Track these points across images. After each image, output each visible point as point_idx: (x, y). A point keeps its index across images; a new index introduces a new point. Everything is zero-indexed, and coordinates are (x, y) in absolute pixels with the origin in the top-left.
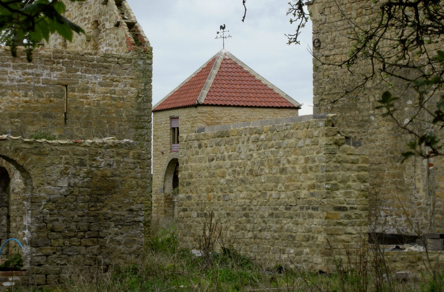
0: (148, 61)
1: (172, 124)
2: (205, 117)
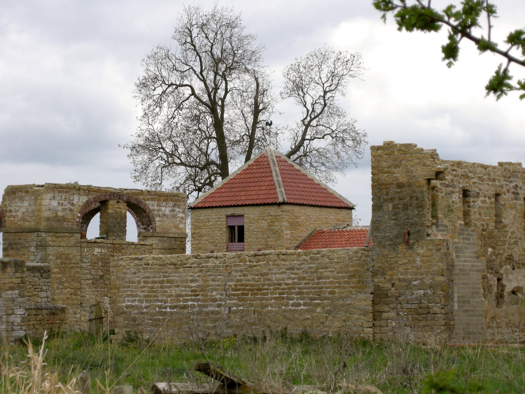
0: (375, 184)
1: (229, 222)
2: (288, 215)
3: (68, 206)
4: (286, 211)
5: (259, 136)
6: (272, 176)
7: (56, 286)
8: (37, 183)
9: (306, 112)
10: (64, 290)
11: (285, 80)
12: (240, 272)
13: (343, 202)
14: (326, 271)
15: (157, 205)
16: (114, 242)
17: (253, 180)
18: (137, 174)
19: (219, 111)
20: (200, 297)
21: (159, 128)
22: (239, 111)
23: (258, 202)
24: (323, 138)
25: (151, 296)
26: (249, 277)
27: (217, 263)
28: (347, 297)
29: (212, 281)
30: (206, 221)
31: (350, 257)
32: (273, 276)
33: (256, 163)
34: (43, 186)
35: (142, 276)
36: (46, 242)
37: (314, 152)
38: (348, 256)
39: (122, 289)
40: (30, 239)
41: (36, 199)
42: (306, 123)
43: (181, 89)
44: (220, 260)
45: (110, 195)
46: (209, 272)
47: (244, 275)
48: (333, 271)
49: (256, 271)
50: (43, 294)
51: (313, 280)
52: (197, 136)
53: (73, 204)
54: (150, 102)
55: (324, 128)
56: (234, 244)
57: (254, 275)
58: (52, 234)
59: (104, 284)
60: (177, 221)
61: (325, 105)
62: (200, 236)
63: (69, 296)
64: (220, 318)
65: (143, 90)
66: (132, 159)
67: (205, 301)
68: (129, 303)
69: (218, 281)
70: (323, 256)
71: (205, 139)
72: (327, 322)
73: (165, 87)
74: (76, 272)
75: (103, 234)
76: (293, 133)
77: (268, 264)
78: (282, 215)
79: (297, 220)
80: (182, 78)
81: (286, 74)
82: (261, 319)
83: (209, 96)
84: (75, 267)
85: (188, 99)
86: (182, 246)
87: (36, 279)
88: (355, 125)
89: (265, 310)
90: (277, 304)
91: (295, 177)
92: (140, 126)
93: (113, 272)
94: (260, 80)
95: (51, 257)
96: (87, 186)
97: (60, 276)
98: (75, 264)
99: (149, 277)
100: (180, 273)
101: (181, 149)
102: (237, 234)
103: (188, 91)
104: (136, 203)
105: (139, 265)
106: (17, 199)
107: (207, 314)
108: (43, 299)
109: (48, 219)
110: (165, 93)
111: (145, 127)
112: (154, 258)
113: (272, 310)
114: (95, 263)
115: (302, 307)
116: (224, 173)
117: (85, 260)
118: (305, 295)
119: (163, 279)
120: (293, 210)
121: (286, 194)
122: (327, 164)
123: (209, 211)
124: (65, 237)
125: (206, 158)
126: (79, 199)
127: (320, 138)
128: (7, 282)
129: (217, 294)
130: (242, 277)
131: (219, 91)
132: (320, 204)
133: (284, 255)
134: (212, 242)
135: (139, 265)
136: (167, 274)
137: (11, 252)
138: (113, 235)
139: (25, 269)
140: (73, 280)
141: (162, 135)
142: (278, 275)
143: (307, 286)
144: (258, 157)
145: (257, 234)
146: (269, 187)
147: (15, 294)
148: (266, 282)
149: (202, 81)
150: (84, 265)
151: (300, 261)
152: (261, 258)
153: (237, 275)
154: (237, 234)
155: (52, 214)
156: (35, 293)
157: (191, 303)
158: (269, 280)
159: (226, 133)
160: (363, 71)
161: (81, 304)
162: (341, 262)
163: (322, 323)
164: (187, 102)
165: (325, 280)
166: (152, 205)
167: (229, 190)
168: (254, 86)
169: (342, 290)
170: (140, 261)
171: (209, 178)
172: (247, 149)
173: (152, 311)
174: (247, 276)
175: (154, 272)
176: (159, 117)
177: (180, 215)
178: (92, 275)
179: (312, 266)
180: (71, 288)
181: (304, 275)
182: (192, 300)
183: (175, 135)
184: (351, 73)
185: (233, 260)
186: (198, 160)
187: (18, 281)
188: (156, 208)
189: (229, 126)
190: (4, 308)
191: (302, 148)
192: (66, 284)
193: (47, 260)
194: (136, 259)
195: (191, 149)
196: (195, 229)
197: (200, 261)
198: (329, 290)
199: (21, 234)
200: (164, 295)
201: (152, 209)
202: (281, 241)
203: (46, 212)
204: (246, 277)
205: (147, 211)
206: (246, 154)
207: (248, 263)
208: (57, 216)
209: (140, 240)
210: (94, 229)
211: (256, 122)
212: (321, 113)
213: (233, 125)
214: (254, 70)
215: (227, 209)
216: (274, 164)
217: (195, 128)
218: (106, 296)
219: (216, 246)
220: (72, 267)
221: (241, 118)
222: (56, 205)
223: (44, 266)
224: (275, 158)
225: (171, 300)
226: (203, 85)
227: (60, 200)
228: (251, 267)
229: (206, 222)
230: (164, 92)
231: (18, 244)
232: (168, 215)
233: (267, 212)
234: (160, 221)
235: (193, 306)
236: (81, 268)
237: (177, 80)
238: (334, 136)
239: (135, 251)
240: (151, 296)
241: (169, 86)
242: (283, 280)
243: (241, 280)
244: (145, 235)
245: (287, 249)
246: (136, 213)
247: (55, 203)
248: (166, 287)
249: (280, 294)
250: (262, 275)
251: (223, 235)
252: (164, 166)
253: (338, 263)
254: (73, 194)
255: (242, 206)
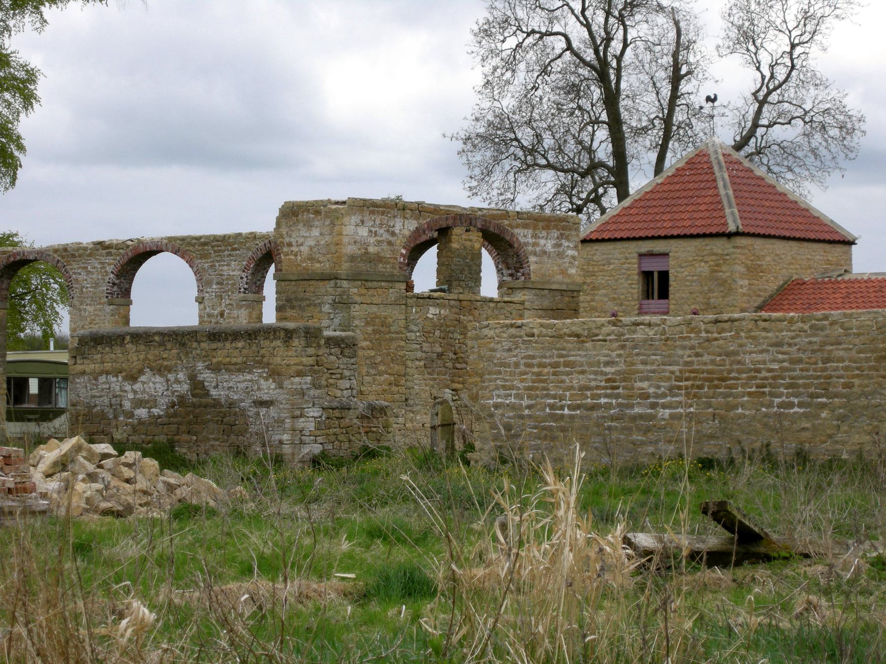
1: (643, 265)
2: (744, 254)
3: (386, 236)
4: (741, 247)
5: (680, 119)
6: (716, 188)
7: (364, 370)
8: (334, 198)
9: (760, 79)
10: (378, 377)
11: (725, 24)
12: (690, 349)
13: (837, 232)
14: (838, 349)
15: (532, 236)
16: (461, 297)
17: (684, 194)
18: (474, 184)
19: (612, 77)
20: (620, 391)
21: (510, 106)
22: (647, 77)
23: (694, 231)
24: (789, 123)
25: (537, 388)
26: (706, 358)
27: (651, 333)
28: (874, 393)
29: (642, 363)
30: (604, 262)
31: (879, 325)
32: (747, 356)
33: (690, 166)
34: (344, 203)
35: (523, 355)
36: (348, 295)
37: (776, 147)
38: (876, 323)
39: (487, 376)
40: (323, 291)
41: (333, 224)
42: (761, 98)
43: (549, 39)
44: (656, 328)
45: (455, 218)
46: (636, 348)
47: (697, 355)
48: (850, 349)
49: (718, 347)
50: (345, 384)
51: (816, 363)
52: (576, 119)
53: (393, 234)
54: (496, 61)
55: (792, 108)
56: (651, 301)
57: (714, 354)
58: (360, 283)
59: (445, 367)
60: (565, 263)
61: (793, 67)
62: (594, 288)
63: (386, 387)
64: (655, 426)
65: (484, 42)
66: (464, 158)
67: (629, 397)
68: (499, 400)
69: (652, 364)
70: (832, 324)
71: (588, 124)
72: (840, 435)
73: (521, 36)
74: (399, 346)
75: (442, 284)
76: (738, 114)
77: (737, 336)
78: (734, 253)
79: (760, 263)
80: (551, 22)
81: (727, 15)
82: (726, 428)
83: (596, 52)
84: (397, 339)
85: (560, 56)
86: (573, 306)
87: (333, 358)
88: (845, 101)
89: (731, 414)
90: (753, 404)
91: (758, 193)
92: (479, 102)
93: (473, 347)
94: (682, 24)
95: (357, 322)
96: (416, 203)
97: (372, 353)
98: (397, 333)
99: (533, 357)
100: (587, 350)
101: (548, 141)
102: (656, 285)
103: (560, 44)
104: (496, 231)
105: (517, 337)
106: (301, 225)
107: (634, 418)
108: (345, 392)
109: (352, 258)
110: (521, 47)
111: (486, 104)
112: (542, 325)
113: (744, 415)
114: (429, 332)
115: (796, 409)
116: (621, 183)
117: (413, 327)
118: (801, 390)
119: (558, 360)
120: (752, 245)
121: (741, 218)
122: (797, 170)
123: (609, 246)
124: (381, 288)
125: (590, 158)
126: (403, 225)
127: (783, 124)
128: (292, 363)
129: (650, 386)
130: (693, 358)
131: (613, 43)
132: (798, 235)
133: (765, 320)
134: (614, 299)
135: (517, 337)
136: (564, 352)
137: (289, 313)
138: (460, 286)
139: (322, 342)
140: (393, 360)
141: (517, 117)
142: (754, 355)
143: (804, 374)
144: (693, 155)
145: (691, 285)
146: (713, 207)
147: (306, 383)
148: (735, 367)
149: (585, 26)
150: (412, 336)
151: (794, 331)
152: (726, 326)
153: (686, 355)
154: (656, 285)
155: (359, 249)
156: (331, 381)
157: (606, 400)
158: (739, 362)
159: (624, 115)
160: (857, 9)
161: (406, 400)
162: (863, 334)
163: (830, 436)
164: (559, 62)
165: (836, 364)
166: (523, 236)
167: (643, 211)
168: (672, 34)
169: (866, 382)
170: (518, 329)
171: (595, 190)
172: (660, 142)
173: (538, 413)
174: (702, 356)
175: (543, 348)
176: (511, 88)
177: (570, 252)
178: (425, 352)
179: (814, 339)
180: (389, 374)
181: (801, 355)
182: (606, 396)
183: (537, 117)
184: (837, 12)
185: (678, 329)
186: (576, 161)
187: (311, 361)
188: (530, 241)
189: (630, 103)
190: (287, 406)
191: (753, 140)
192: (382, 368)
193: (350, 326)
194: (512, 326)
195: (565, 141)
196: (585, 276)
197: (621, 330)
198: (842, 380)
199: (306, 282)
200: (560, 387)
201: (524, 243)
202: (732, 297)
203: (350, 247)
204: (700, 358)
205: (516, 245)
206: (658, 150)
207: (704, 334)
208: (367, 253)
209: (501, 295)
210: (426, 274)
211: (675, 95)
212: (785, 81)
213: (637, 101)
214: (672, 8)
215: (640, 243)
216: (720, 167)
217: (572, 105)
218: (447, 387)
219: (621, 305)
220: (392, 339)
221: (650, 89)
222: (366, 234)
223: (347, 337)
224: (721, 158)
225: (572, 395)
226: (586, 34)
227: (372, 226)
228: (708, 341)
229: (604, 265)
230: (519, 45)
231: (302, 299)
232: (550, 252)
233: (709, 247)
234: (536, 263)
235: (608, 406)
236: (407, 340)
237: (542, 24)
238: (807, 119)
239: (496, 312)
240: (537, 388)
241: (528, 35)
242: (764, 362)
243: (692, 363)
244: (511, 285)
245: (743, 310)
246: (496, 249)
247: (363, 232)
248: (563, 373)
249: (758, 387)
250: (728, 354)
251: (633, 287)
252: (519, 171)
253: (859, 335)
254: (394, 217)
255: (666, 237)
